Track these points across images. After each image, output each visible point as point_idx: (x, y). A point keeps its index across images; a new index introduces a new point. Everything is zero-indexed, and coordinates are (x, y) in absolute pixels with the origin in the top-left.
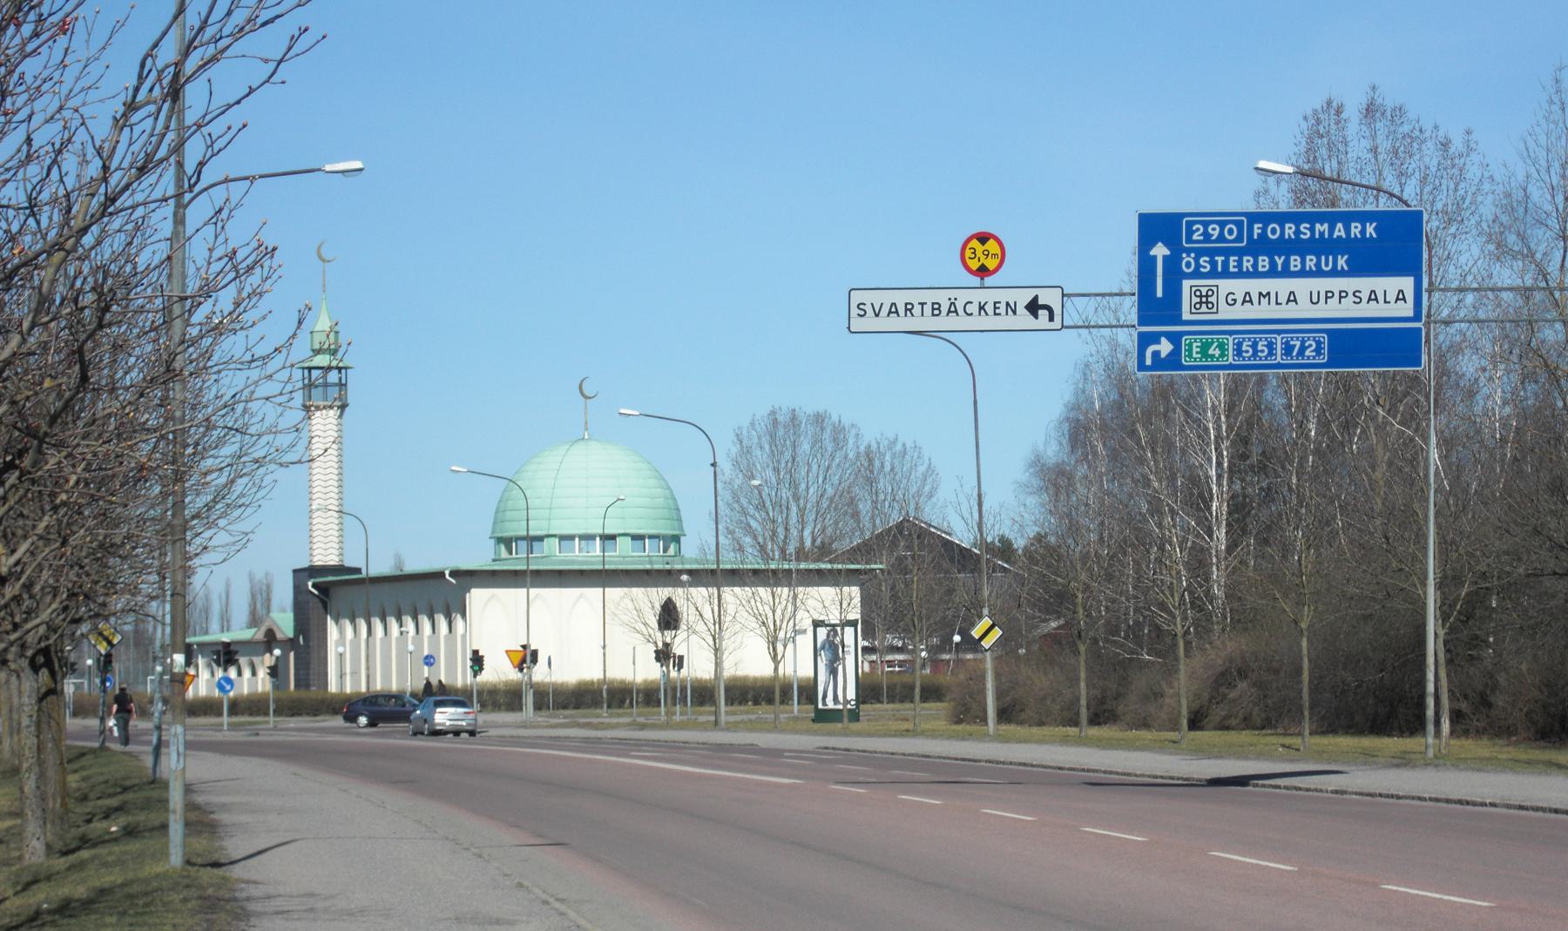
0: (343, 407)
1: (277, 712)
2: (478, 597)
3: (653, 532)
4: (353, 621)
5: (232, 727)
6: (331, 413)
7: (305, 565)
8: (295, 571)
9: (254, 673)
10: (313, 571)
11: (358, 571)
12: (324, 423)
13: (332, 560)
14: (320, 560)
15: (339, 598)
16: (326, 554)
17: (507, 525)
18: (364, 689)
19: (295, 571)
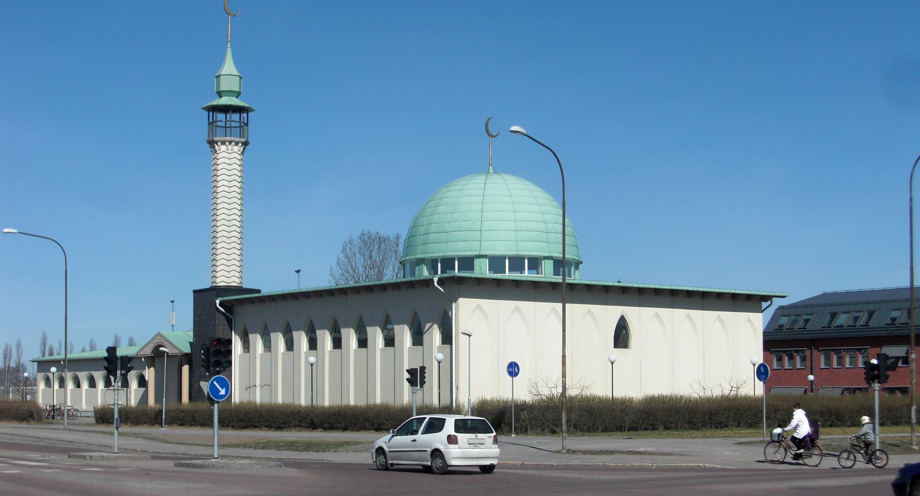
0: (245, 144)
1: (223, 424)
2: (467, 311)
3: (547, 254)
4: (387, 326)
5: (68, 424)
6: (236, 148)
7: (207, 285)
8: (195, 292)
9: (78, 385)
10: (217, 291)
11: (259, 291)
12: (229, 157)
13: (234, 282)
14: (221, 282)
15: (243, 315)
16: (227, 277)
17: (431, 246)
18: (303, 402)
19: (195, 292)
